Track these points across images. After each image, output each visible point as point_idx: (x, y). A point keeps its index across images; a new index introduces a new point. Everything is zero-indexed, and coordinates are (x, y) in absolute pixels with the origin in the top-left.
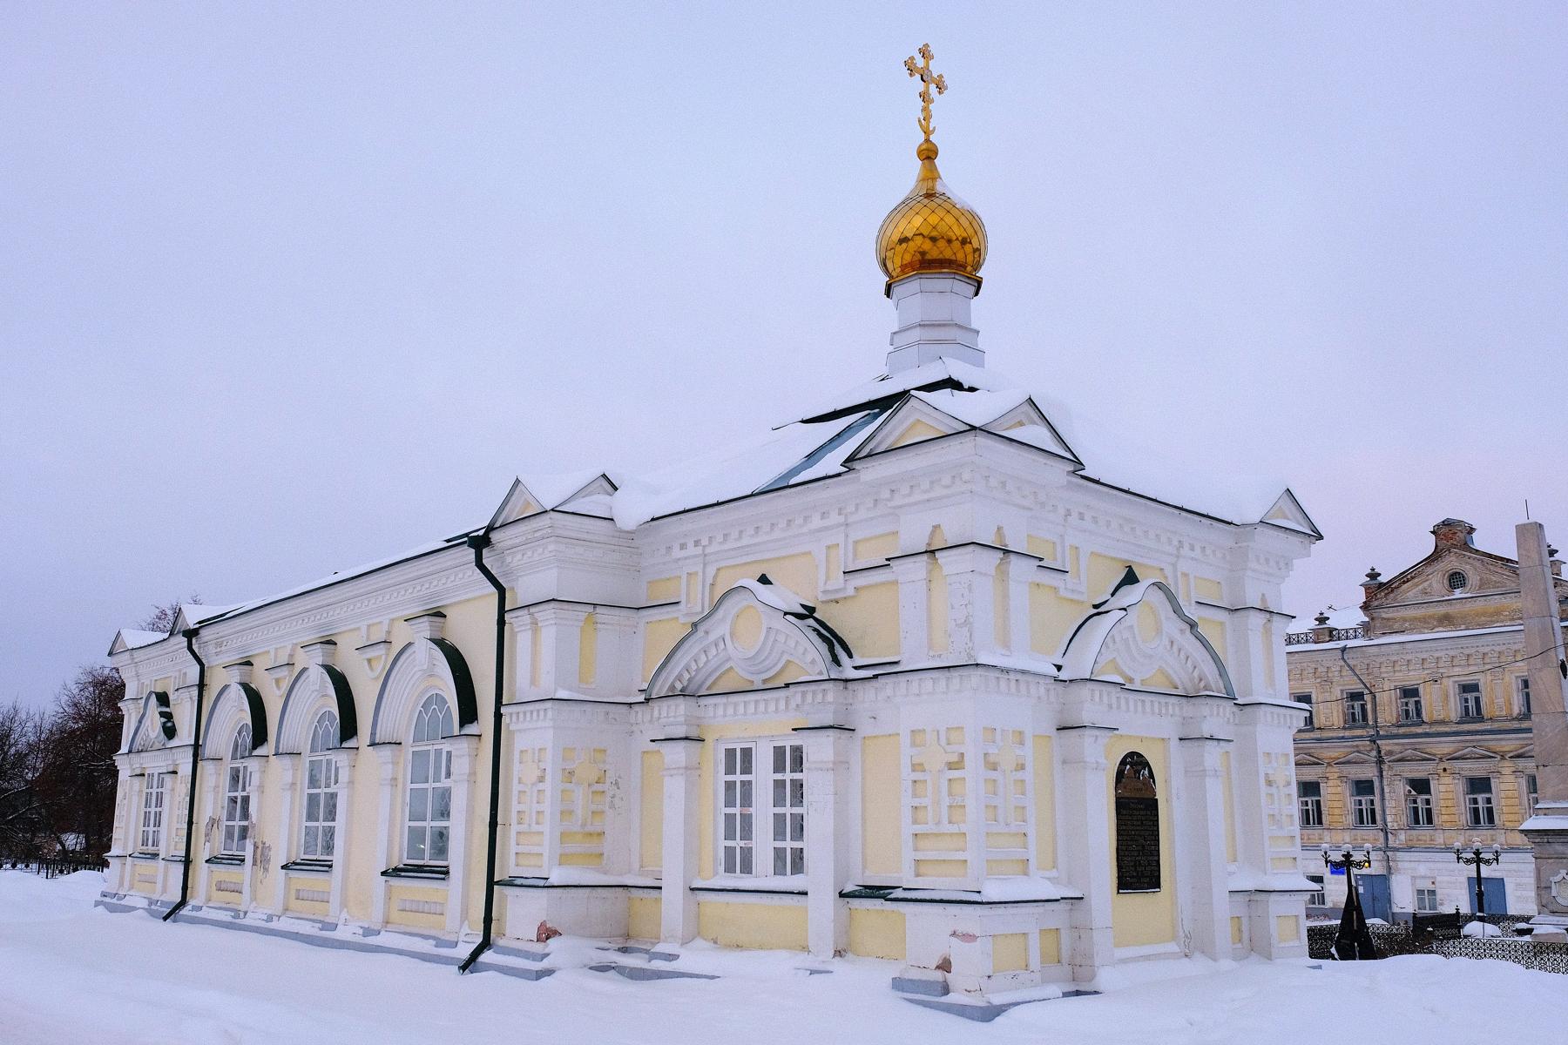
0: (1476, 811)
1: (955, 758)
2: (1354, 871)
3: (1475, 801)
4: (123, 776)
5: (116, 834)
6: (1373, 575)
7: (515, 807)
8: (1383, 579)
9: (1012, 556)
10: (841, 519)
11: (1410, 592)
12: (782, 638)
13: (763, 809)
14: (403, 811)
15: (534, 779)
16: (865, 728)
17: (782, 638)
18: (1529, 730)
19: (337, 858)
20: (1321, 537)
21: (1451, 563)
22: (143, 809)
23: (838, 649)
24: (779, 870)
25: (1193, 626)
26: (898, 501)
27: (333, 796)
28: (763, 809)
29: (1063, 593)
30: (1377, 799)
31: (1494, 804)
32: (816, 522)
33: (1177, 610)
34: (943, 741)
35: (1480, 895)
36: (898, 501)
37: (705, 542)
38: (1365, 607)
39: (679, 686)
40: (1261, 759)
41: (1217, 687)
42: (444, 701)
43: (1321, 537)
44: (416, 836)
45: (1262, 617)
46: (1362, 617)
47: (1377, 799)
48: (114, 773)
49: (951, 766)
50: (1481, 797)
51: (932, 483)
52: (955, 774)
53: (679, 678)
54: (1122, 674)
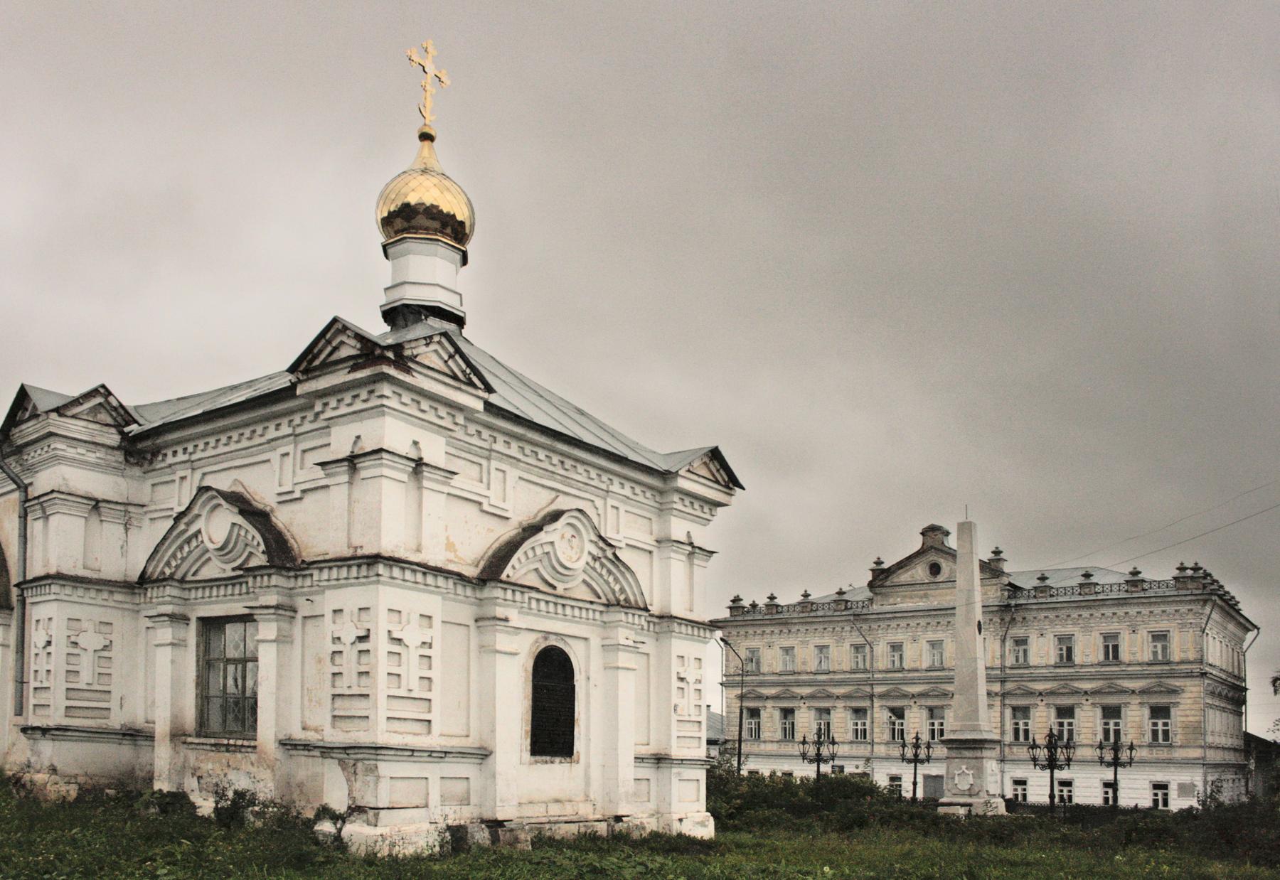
0: (933, 731)
1: (362, 633)
6: (879, 563)
7: (33, 668)
8: (885, 566)
10: (290, 431)
11: (904, 577)
12: (243, 533)
15: (42, 644)
16: (304, 609)
17: (243, 533)
18: (279, 494)
21: (933, 557)
26: (329, 414)
29: (486, 507)
30: (868, 722)
31: (945, 727)
32: (272, 433)
34: (355, 619)
36: (329, 414)
37: (190, 449)
38: (871, 585)
39: (168, 572)
40: (675, 661)
46: (869, 594)
49: (362, 639)
51: (339, 401)
52: (363, 646)
53: (168, 564)
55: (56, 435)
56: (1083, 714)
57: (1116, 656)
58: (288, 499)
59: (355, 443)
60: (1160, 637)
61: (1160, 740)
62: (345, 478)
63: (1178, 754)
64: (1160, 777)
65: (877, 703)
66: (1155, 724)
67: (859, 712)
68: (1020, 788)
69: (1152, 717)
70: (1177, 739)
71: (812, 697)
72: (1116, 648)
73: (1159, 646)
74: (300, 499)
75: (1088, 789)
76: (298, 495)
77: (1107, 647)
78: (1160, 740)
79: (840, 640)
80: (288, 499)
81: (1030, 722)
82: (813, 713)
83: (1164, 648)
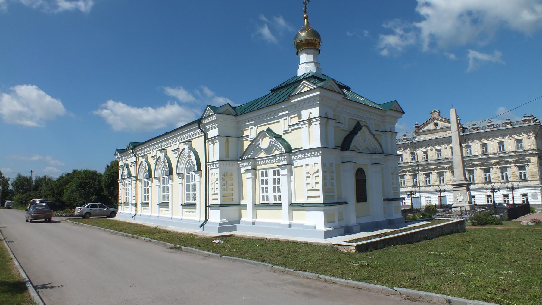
2: (412, 196)
3: (486, 175)
4: (120, 184)
5: (120, 198)
9: (330, 120)
13: (271, 186)
14: (288, 273)
19: (170, 202)
20: (404, 113)
22: (150, 194)
23: (48, 286)
24: (275, 200)
25: (374, 135)
27: (168, 187)
28: (271, 186)
33: (370, 132)
35: (441, 200)
41: (380, 151)
42: (192, 163)
43: (404, 113)
44: (188, 196)
45: (391, 133)
47: (418, 179)
48: (118, 183)
50: (487, 174)
54: (357, 148)
55: (338, 85)
56: (511, 169)
57: (503, 149)
58: (286, 132)
59: (309, 115)
60: (519, 141)
61: (523, 178)
62: (308, 125)
63: (529, 183)
64: (524, 192)
65: (420, 173)
66: (521, 173)
67: (414, 176)
68: (506, 198)
69: (519, 170)
70: (528, 178)
71: (435, 169)
72: (503, 147)
73: (519, 144)
74: (290, 132)
75: (481, 199)
76: (290, 131)
77: (500, 147)
78: (523, 178)
79: (509, 140)
80: (286, 132)
81: (474, 175)
82: (499, 170)
83: (521, 145)
